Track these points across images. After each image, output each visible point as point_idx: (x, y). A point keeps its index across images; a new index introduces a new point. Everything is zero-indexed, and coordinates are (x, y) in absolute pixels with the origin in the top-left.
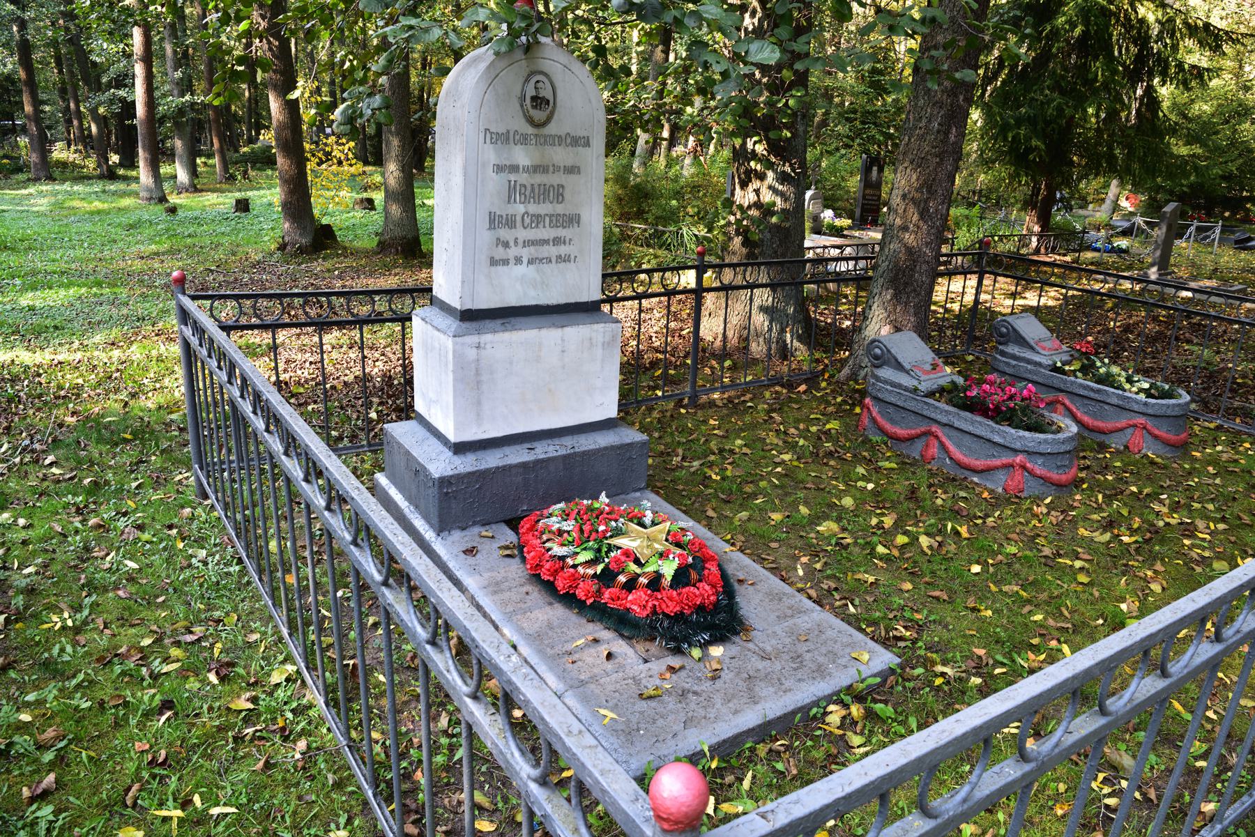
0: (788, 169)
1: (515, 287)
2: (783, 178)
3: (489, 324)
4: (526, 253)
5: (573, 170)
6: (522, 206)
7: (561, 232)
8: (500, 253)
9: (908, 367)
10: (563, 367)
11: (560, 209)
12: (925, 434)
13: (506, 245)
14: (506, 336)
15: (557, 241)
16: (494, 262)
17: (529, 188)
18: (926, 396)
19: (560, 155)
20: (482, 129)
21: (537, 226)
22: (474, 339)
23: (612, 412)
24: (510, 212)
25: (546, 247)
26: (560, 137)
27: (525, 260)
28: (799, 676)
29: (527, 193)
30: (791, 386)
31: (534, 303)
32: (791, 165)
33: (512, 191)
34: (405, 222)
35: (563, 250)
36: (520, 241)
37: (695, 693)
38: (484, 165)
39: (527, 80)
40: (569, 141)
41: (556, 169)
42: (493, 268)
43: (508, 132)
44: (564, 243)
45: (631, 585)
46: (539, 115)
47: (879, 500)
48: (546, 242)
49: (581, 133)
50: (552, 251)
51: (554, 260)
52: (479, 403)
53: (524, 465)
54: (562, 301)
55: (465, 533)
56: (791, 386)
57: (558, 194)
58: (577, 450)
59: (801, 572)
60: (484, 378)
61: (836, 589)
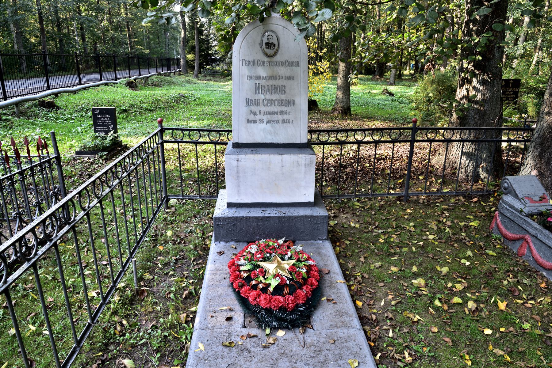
0: (486, 77)
1: (260, 133)
2: (483, 83)
3: (246, 150)
4: (265, 118)
8: (252, 117)
9: (520, 196)
11: (283, 97)
12: (522, 239)
13: (255, 114)
14: (252, 157)
15: (282, 113)
16: (248, 121)
18: (527, 216)
19: (283, 71)
20: (241, 59)
21: (271, 105)
22: (235, 157)
23: (312, 199)
24: (257, 98)
25: (276, 116)
26: (282, 62)
27: (265, 121)
28: (309, 362)
29: (265, 89)
30: (468, 198)
31: (270, 142)
32: (488, 75)
33: (257, 88)
34: (344, 100)
35: (285, 117)
37: (249, 352)
38: (242, 76)
39: (264, 35)
40: (287, 64)
41: (281, 78)
42: (249, 124)
43: (254, 60)
44: (286, 114)
45: (255, 287)
46: (270, 52)
47: (466, 273)
50: (280, 117)
51: (280, 122)
52: (239, 186)
53: (257, 218)
55: (227, 244)
56: (468, 198)
57: (282, 90)
58: (286, 215)
59: (382, 303)
60: (241, 175)
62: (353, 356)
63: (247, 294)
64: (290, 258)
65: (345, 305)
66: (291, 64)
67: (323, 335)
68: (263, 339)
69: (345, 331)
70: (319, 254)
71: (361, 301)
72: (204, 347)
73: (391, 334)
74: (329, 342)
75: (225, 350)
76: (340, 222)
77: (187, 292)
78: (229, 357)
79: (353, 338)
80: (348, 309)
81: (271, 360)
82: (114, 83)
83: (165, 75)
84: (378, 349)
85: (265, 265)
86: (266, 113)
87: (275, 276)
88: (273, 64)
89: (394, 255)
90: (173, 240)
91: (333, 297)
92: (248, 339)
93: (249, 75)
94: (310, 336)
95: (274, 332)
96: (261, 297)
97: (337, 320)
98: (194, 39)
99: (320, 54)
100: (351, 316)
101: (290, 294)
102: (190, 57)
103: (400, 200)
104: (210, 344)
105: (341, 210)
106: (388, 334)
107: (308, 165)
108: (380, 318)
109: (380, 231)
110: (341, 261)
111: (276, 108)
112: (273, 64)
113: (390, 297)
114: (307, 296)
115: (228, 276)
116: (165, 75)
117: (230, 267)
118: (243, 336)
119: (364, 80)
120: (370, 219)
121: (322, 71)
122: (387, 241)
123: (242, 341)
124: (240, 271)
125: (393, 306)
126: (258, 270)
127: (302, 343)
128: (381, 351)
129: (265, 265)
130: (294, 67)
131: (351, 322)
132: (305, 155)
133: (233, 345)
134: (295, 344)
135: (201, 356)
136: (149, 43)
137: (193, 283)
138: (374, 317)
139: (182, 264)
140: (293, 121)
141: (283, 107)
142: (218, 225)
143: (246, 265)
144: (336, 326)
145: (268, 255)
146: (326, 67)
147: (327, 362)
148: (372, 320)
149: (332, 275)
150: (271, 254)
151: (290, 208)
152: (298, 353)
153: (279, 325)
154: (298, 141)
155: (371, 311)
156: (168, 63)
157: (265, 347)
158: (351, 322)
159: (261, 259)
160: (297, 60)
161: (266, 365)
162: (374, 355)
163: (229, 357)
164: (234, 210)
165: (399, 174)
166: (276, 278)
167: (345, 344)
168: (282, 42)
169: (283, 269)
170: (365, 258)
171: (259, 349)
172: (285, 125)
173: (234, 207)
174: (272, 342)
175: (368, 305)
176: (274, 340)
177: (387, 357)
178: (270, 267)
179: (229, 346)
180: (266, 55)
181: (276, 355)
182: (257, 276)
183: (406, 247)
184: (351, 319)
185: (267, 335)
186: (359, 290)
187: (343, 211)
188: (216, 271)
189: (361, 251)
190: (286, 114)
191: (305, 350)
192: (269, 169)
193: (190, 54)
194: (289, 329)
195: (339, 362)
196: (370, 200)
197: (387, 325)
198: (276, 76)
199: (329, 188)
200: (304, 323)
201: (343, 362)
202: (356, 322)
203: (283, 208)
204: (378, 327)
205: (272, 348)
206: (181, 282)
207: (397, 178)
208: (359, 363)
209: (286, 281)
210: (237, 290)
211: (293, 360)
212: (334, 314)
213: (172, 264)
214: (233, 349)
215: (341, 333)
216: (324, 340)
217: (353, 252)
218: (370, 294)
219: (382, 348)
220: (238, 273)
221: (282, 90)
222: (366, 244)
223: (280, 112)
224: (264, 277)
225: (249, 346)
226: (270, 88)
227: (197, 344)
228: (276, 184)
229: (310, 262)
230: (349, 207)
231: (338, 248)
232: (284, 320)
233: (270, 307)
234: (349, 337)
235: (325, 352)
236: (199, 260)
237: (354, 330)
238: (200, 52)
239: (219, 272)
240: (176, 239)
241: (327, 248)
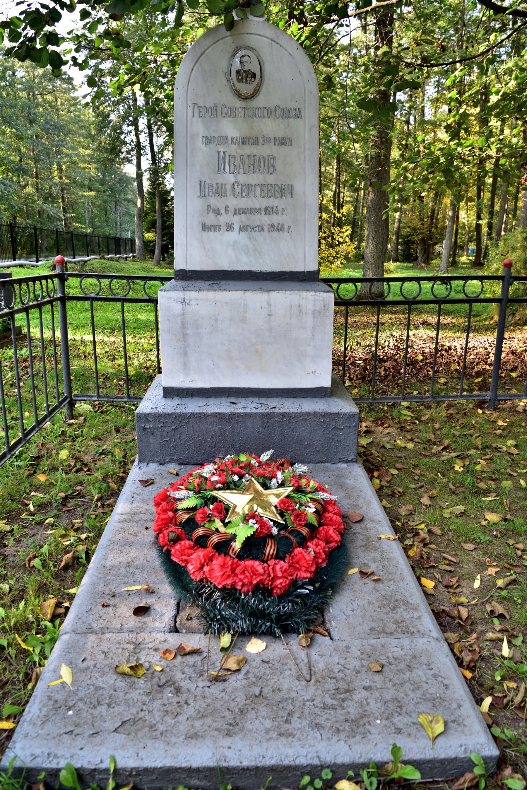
3: (198, 283)
4: (237, 221)
5: (283, 141)
6: (232, 176)
7: (273, 202)
8: (211, 219)
10: (270, 330)
11: (271, 179)
14: (211, 295)
15: (269, 211)
16: (205, 227)
17: (238, 159)
19: (270, 127)
20: (190, 103)
21: (248, 195)
23: (327, 383)
24: (220, 181)
25: (257, 216)
26: (269, 109)
27: (236, 227)
28: (321, 720)
31: (246, 268)
33: (221, 162)
35: (276, 219)
36: (231, 209)
37: (178, 690)
39: (233, 56)
40: (278, 113)
41: (266, 140)
42: (205, 234)
44: (277, 212)
46: (246, 88)
48: (257, 211)
49: (292, 105)
50: (265, 220)
51: (266, 229)
52: (185, 354)
53: (220, 416)
54: (276, 268)
55: (163, 467)
57: (269, 165)
58: (277, 410)
59: (477, 584)
60: (190, 331)
61: (501, 617)
62: (430, 705)
63: (184, 557)
64: (282, 485)
65: (401, 584)
66: (286, 113)
67: (355, 651)
68: (214, 658)
69: (406, 642)
70: (342, 486)
71: (431, 579)
72: (73, 674)
73: (506, 651)
74: (369, 669)
75: (121, 683)
76: (378, 440)
77: (70, 555)
78: (127, 702)
79: (424, 659)
80: (407, 594)
81: (227, 713)
82: (33, 266)
83: (111, 259)
84: (481, 685)
85: (228, 497)
86: (238, 211)
87: (246, 519)
88: (250, 113)
89: (487, 492)
90: (69, 465)
91: (373, 567)
92: (179, 658)
93: (206, 134)
94: (324, 653)
95: (239, 644)
96: (214, 562)
97: (385, 617)
98: (155, 212)
99: (337, 215)
100: (416, 609)
101: (279, 557)
102: (149, 236)
103: (481, 408)
104: (88, 668)
105: (380, 422)
106: (501, 650)
107: (320, 312)
108: (477, 615)
109: (454, 454)
110: (384, 502)
111: (257, 202)
112: (251, 114)
113: (492, 571)
114: (317, 563)
115: (151, 525)
116: (111, 259)
117: (157, 504)
118: (167, 651)
119: (402, 269)
120: (433, 436)
121: (341, 240)
122: (467, 470)
123: (163, 663)
124: (176, 511)
125: (500, 588)
126: (211, 507)
127: (305, 672)
128: (491, 691)
129: (228, 497)
130: (292, 120)
131: (418, 623)
132: (312, 293)
133: (141, 672)
134: (288, 673)
135: (60, 697)
136: (92, 219)
137: (86, 539)
138: (464, 613)
139: (76, 505)
140: (289, 227)
141: (272, 199)
142: (144, 429)
143: (189, 497)
144: (383, 631)
145: (236, 478)
146: (346, 234)
147: (365, 720)
148: (460, 618)
149: (368, 524)
150: (241, 477)
151: (284, 400)
152: (294, 695)
153: (254, 626)
154: (300, 268)
155: (454, 600)
156: (117, 245)
157: (216, 679)
158: (418, 623)
159: (219, 485)
160: (297, 106)
161: (214, 725)
162: (479, 702)
163: (127, 702)
164: (176, 401)
165: (475, 371)
166: (247, 521)
167: (408, 673)
168: (268, 68)
169: (265, 506)
170: (430, 497)
171: (201, 684)
172: (275, 234)
173: (178, 395)
174: (234, 667)
175: (447, 587)
176: (239, 662)
177: (506, 706)
178: (239, 501)
179: (130, 676)
180: (238, 94)
181: (241, 699)
182: (209, 519)
183: (507, 479)
184: (416, 615)
185: (223, 649)
186: (425, 556)
187: (382, 424)
188: (130, 518)
189: (422, 487)
190: (277, 212)
191: (312, 689)
192: (244, 320)
193: (149, 232)
194: (275, 637)
195: (396, 720)
196: (428, 407)
197: (494, 630)
198: (257, 138)
199: (356, 390)
200: (309, 622)
201: (407, 720)
202: (428, 623)
203: (270, 400)
204: (474, 636)
205: (235, 682)
206: (63, 536)
207: (472, 376)
208: (446, 724)
209: (269, 528)
210: (165, 549)
211: (281, 713)
212: (377, 604)
213: (55, 505)
214: (141, 681)
215: (397, 647)
216: (358, 664)
217: (406, 487)
218: (449, 565)
219: (489, 683)
220: (171, 514)
221: (269, 165)
222: (429, 475)
223: (266, 208)
224: (222, 521)
225: (179, 676)
226: (246, 162)
227: (59, 668)
228: (257, 351)
229: (325, 496)
230: (393, 418)
231: (378, 481)
232: (262, 615)
233: (234, 584)
234: (414, 657)
235: (360, 695)
236: (108, 499)
237: (425, 640)
238: (163, 230)
239: (136, 518)
240: (73, 464)
241: (358, 472)
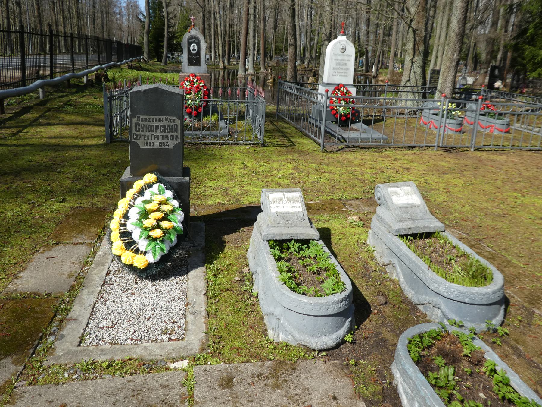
4: (339, 74)
5: (348, 60)
15: (345, 73)
19: (346, 58)
35: (346, 74)
50: (343, 74)
57: (346, 64)
66: (349, 56)
86: (340, 73)
